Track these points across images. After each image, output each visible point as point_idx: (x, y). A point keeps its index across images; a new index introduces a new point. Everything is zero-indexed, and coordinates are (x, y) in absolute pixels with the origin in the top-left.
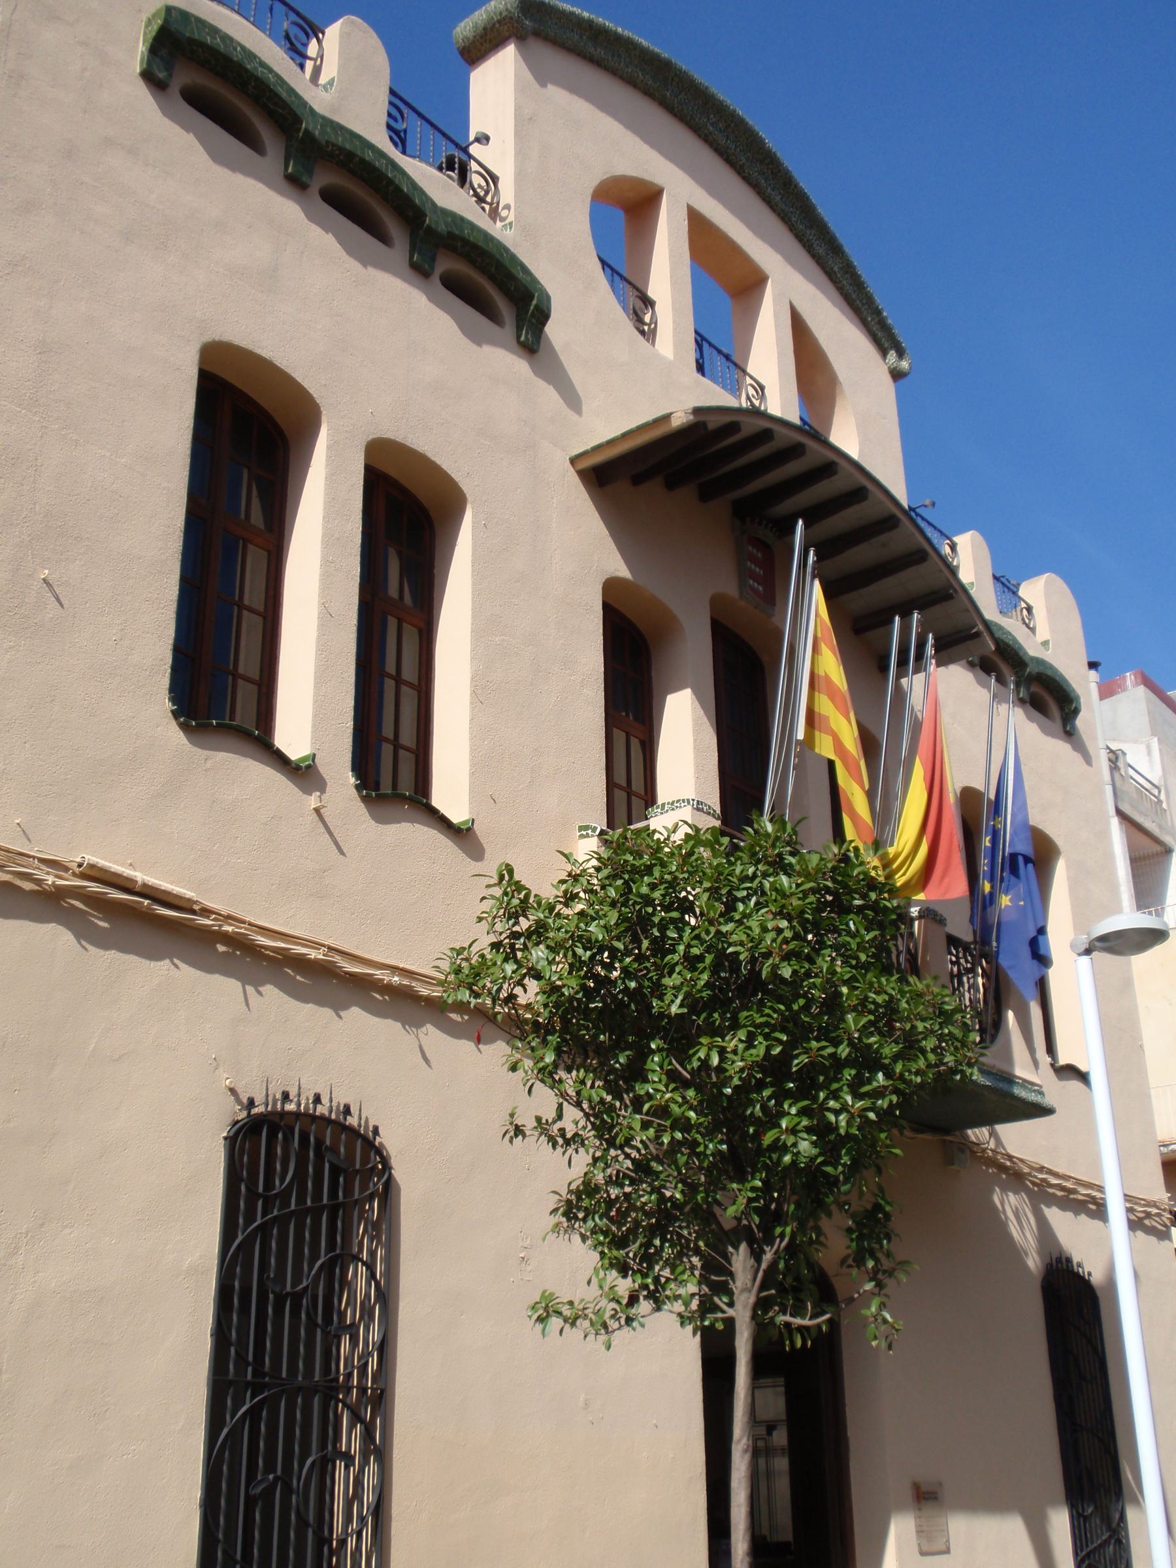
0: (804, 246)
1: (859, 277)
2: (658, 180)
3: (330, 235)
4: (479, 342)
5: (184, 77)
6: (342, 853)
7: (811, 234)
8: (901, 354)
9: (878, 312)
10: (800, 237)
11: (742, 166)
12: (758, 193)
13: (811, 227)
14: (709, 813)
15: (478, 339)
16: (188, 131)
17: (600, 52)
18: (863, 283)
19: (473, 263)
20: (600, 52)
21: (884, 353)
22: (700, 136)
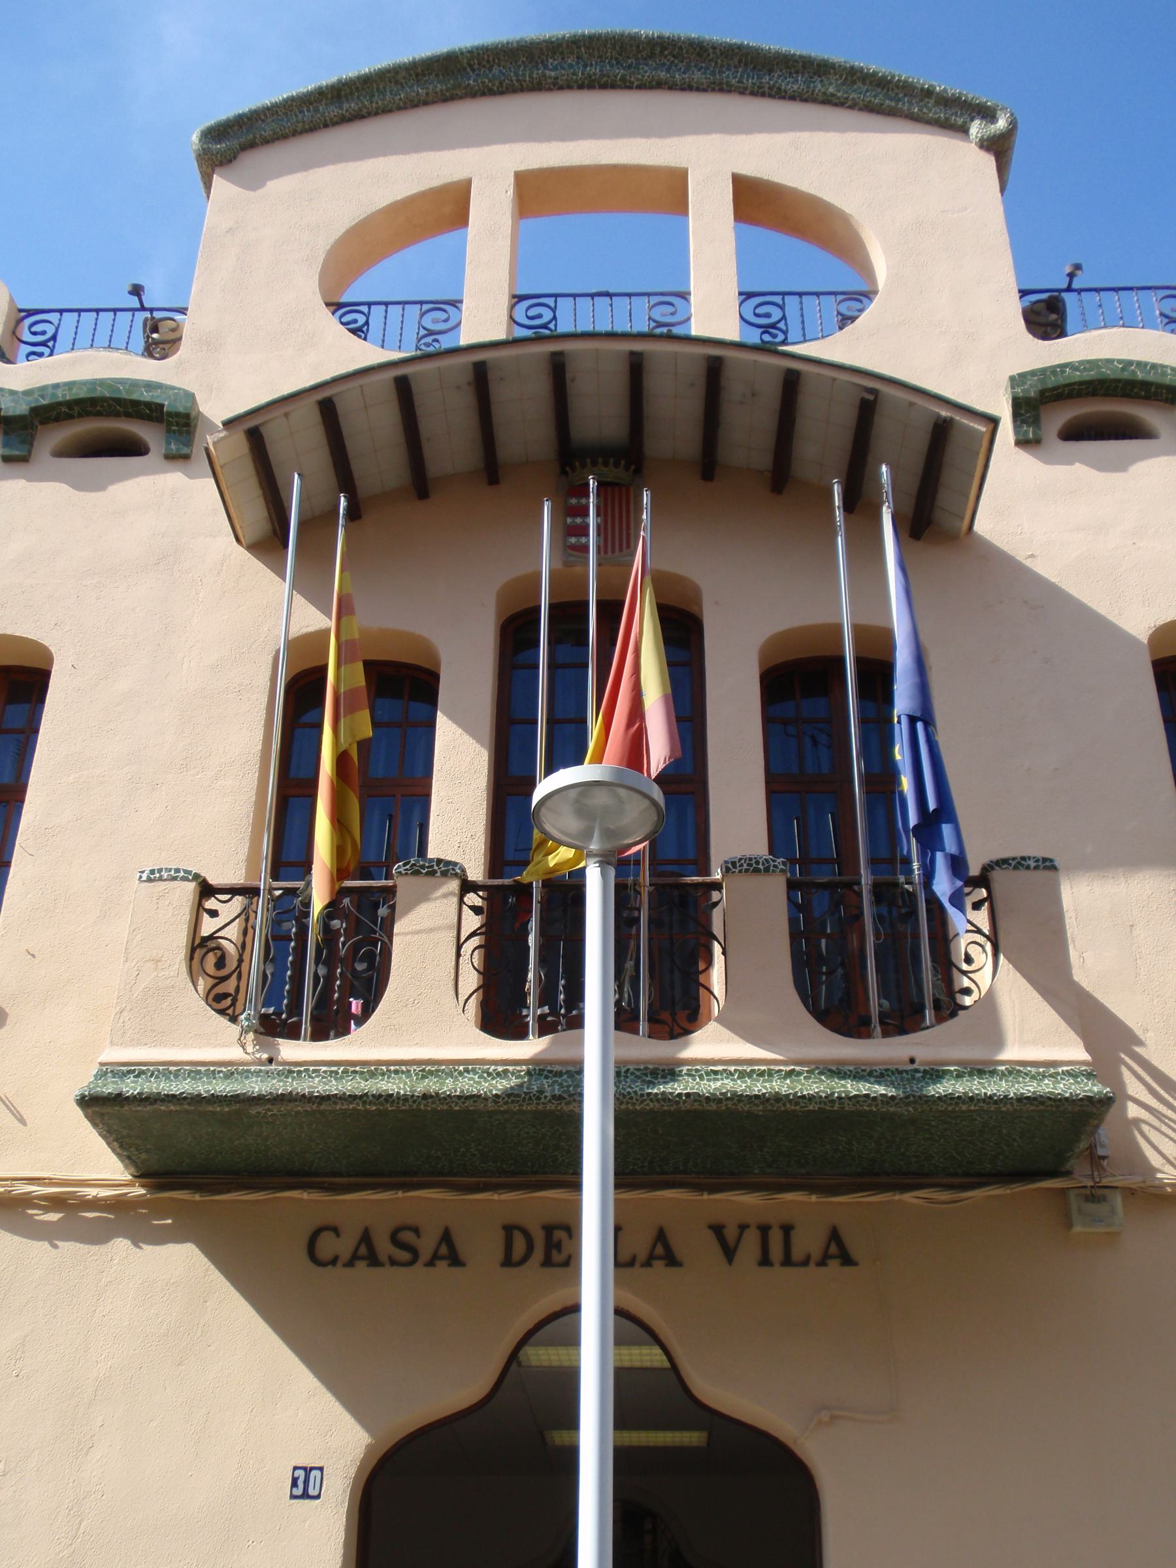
0: (771, 96)
1: (875, 74)
2: (458, 175)
3: (1077, 464)
4: (102, 488)
5: (1057, 418)
6: (23, 1121)
7: (777, 79)
8: (988, 114)
9: (928, 93)
10: (758, 92)
11: (623, 79)
12: (670, 88)
13: (770, 71)
14: (174, 879)
15: (1121, 466)
16: (1071, 463)
17: (351, 106)
18: (884, 77)
19: (99, 414)
20: (351, 106)
21: (964, 130)
22: (550, 89)
